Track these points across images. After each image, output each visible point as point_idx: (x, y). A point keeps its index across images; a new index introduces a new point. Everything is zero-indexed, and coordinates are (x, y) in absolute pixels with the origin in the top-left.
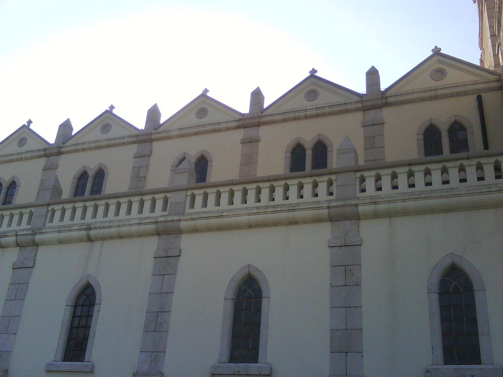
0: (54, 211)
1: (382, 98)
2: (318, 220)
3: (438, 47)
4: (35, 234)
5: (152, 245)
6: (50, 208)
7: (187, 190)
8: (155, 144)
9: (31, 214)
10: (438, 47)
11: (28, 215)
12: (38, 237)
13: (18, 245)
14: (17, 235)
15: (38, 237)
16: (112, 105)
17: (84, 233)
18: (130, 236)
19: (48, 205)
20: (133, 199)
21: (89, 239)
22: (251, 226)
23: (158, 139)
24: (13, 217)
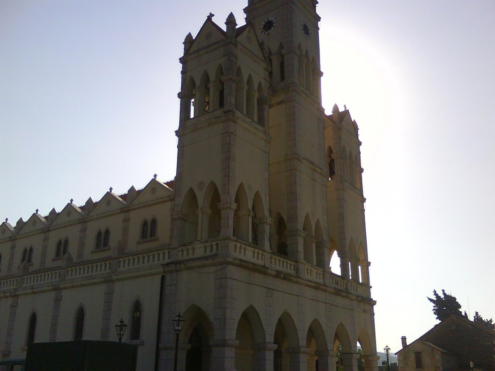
0: (120, 262)
1: (184, 135)
2: (102, 283)
3: (457, 301)
4: (16, 291)
5: (53, 294)
6: (118, 260)
7: (117, 259)
8: (88, 223)
9: (110, 263)
10: (457, 301)
11: (152, 256)
12: (17, 293)
13: (11, 296)
14: (10, 292)
15: (17, 293)
16: (155, 174)
17: (31, 291)
18: (46, 291)
19: (65, 268)
20: (165, 251)
21: (34, 293)
22: (82, 285)
23: (89, 221)
24: (154, 256)
